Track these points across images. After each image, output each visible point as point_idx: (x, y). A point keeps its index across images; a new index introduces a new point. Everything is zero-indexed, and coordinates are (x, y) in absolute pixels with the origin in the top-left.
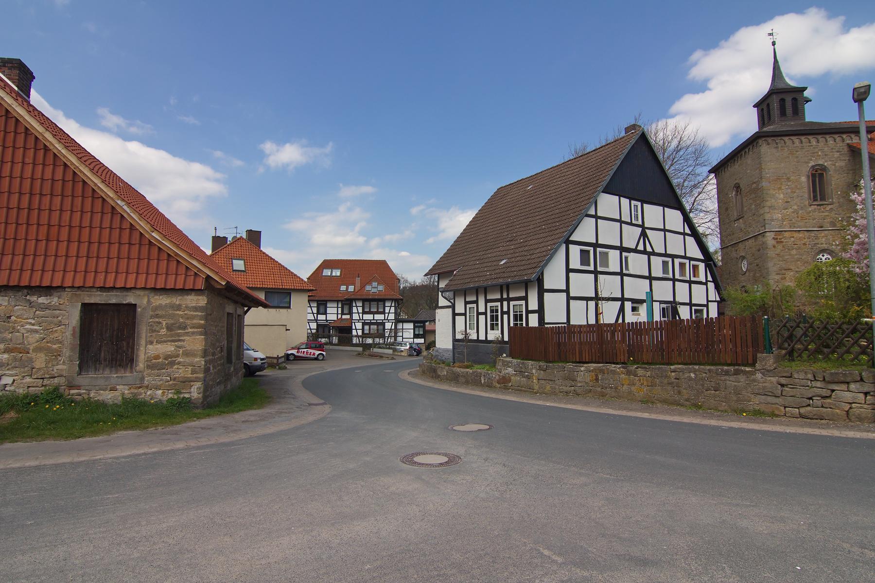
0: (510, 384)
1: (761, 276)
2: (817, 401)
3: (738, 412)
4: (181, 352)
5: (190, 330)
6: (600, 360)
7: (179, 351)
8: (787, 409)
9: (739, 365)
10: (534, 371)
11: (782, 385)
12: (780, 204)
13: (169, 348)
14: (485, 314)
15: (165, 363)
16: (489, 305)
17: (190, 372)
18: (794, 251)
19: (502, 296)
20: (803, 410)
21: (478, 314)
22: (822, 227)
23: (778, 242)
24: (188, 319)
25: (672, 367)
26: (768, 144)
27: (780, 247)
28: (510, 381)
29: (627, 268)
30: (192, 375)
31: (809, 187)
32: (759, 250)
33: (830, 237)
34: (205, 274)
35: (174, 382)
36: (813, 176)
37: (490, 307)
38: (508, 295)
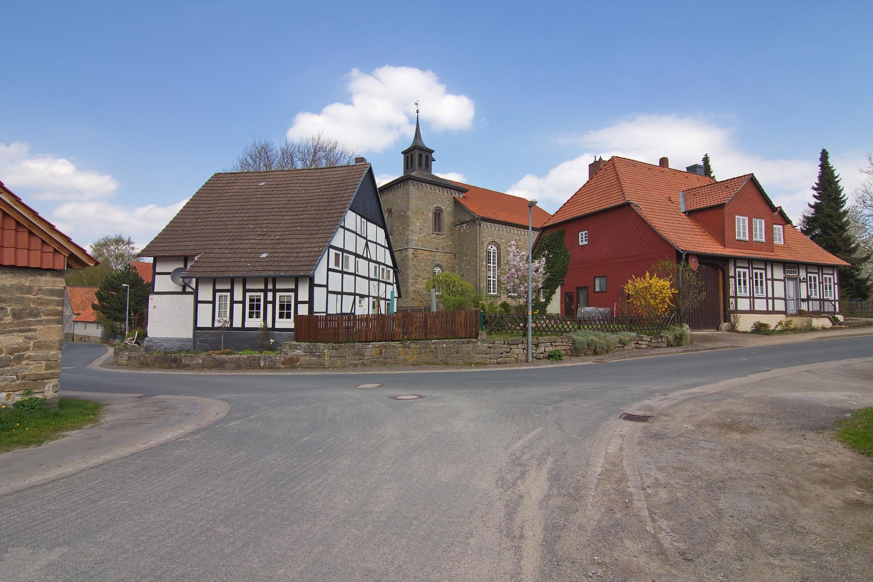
0: (298, 364)
1: (403, 279)
2: (505, 355)
3: (469, 365)
4: (32, 344)
5: (44, 318)
6: (382, 340)
7: (30, 343)
8: (491, 360)
9: (470, 338)
10: (326, 351)
11: (490, 348)
12: (417, 230)
13: (17, 340)
14: (243, 303)
15: (10, 358)
16: (248, 294)
17: (44, 368)
18: (423, 263)
19: (266, 286)
20: (498, 360)
21: (233, 302)
22: (437, 249)
23: (414, 256)
24: (41, 304)
25: (433, 341)
26: (414, 185)
27: (415, 260)
28: (298, 360)
29: (358, 271)
30: (46, 372)
31: (433, 220)
32: (402, 261)
33: (441, 256)
34: (67, 252)
35: (23, 381)
36: (435, 213)
37: (220, 296)
38: (274, 286)
